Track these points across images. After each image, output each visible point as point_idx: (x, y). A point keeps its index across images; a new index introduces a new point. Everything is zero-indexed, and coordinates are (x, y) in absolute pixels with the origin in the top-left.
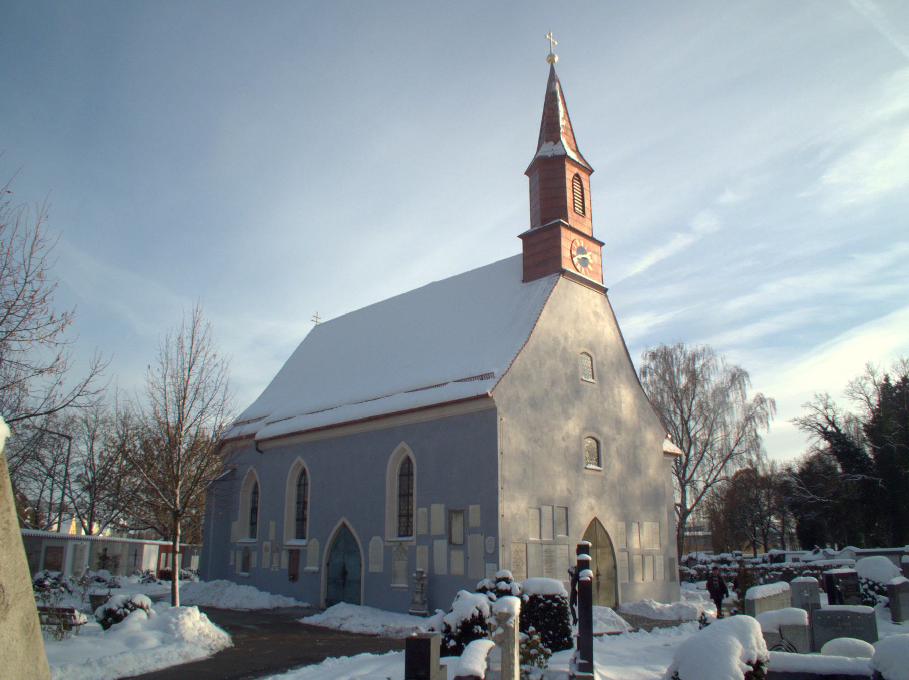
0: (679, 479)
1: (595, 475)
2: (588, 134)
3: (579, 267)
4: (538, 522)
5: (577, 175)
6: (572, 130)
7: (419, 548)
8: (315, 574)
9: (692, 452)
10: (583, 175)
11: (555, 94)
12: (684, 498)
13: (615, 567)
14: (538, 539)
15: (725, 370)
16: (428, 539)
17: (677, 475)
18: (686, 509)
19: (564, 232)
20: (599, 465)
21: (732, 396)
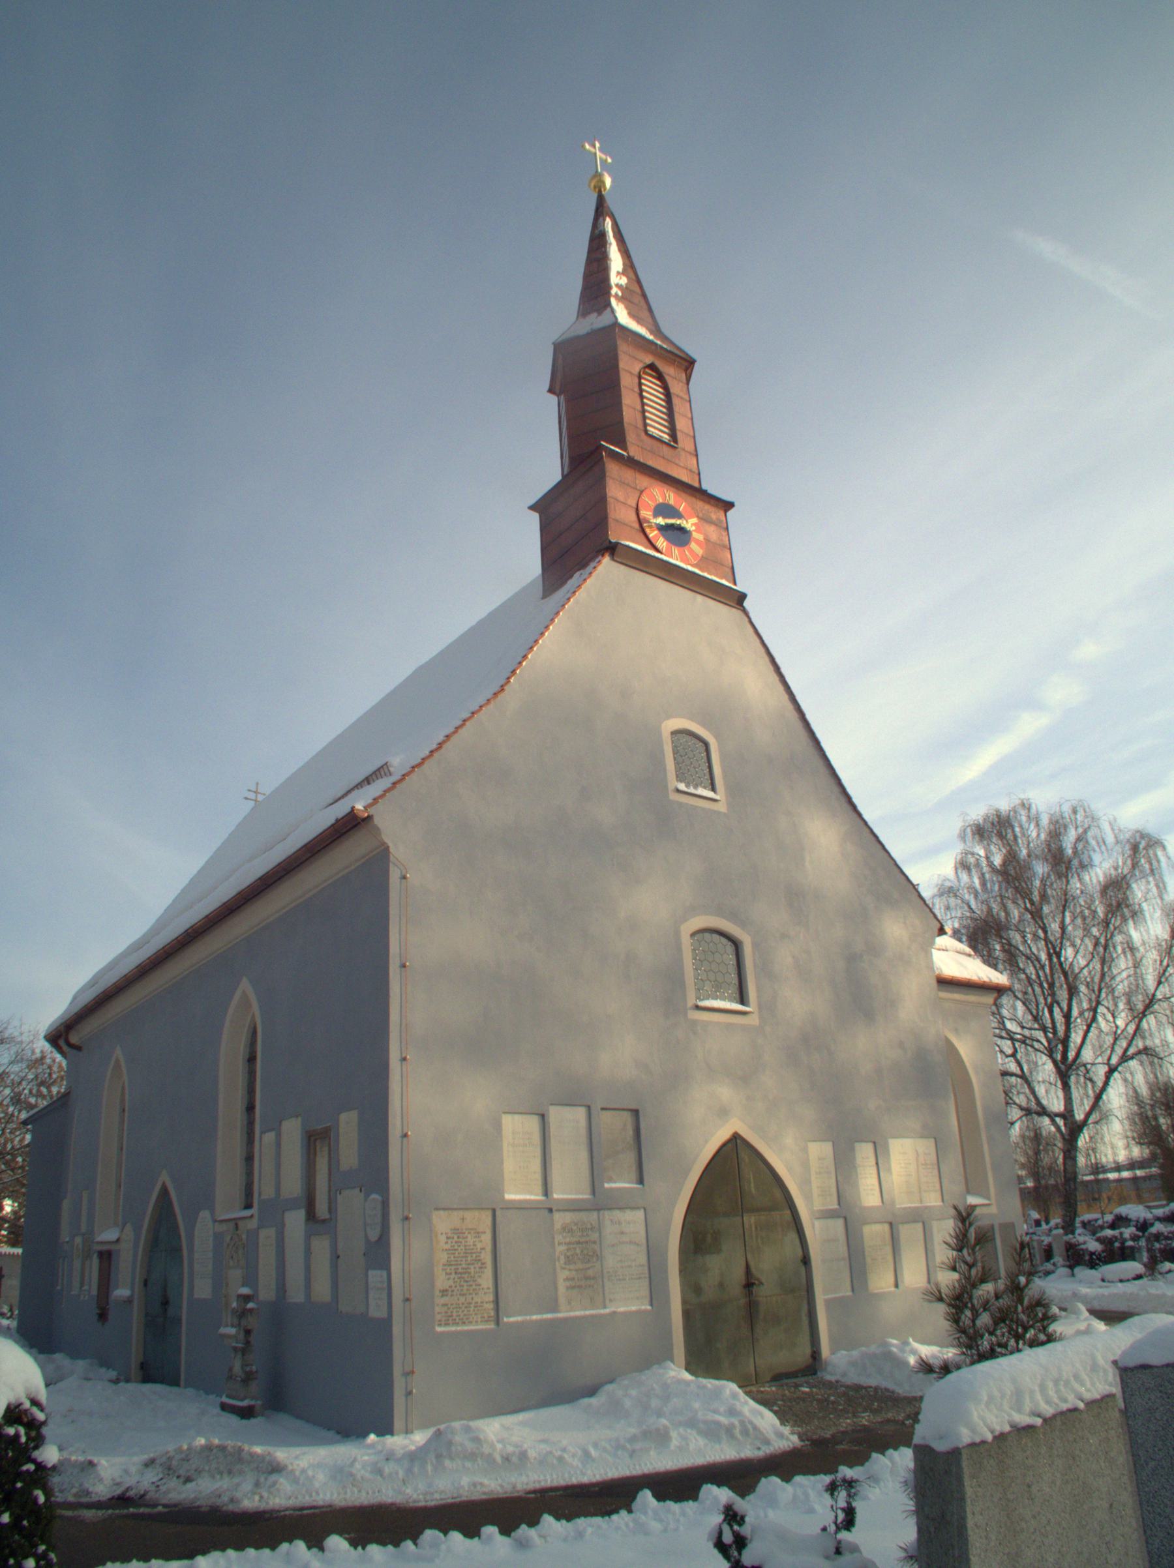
0: (1055, 1062)
1: (729, 1026)
2: (667, 287)
3: (661, 543)
4: (538, 1152)
5: (652, 367)
6: (644, 296)
7: (263, 1233)
8: (129, 1301)
9: (1075, 1012)
10: (669, 371)
11: (603, 235)
12: (1068, 1100)
13: (806, 1261)
14: (536, 1196)
15: (1117, 842)
16: (274, 1212)
17: (1051, 1055)
18: (1074, 1122)
19: (613, 470)
20: (743, 1000)
21: (1138, 890)
